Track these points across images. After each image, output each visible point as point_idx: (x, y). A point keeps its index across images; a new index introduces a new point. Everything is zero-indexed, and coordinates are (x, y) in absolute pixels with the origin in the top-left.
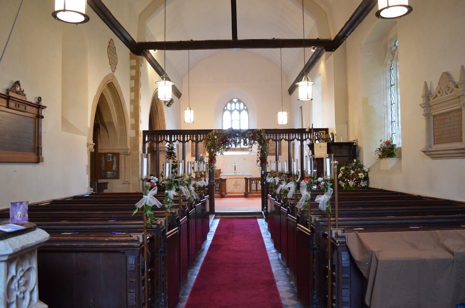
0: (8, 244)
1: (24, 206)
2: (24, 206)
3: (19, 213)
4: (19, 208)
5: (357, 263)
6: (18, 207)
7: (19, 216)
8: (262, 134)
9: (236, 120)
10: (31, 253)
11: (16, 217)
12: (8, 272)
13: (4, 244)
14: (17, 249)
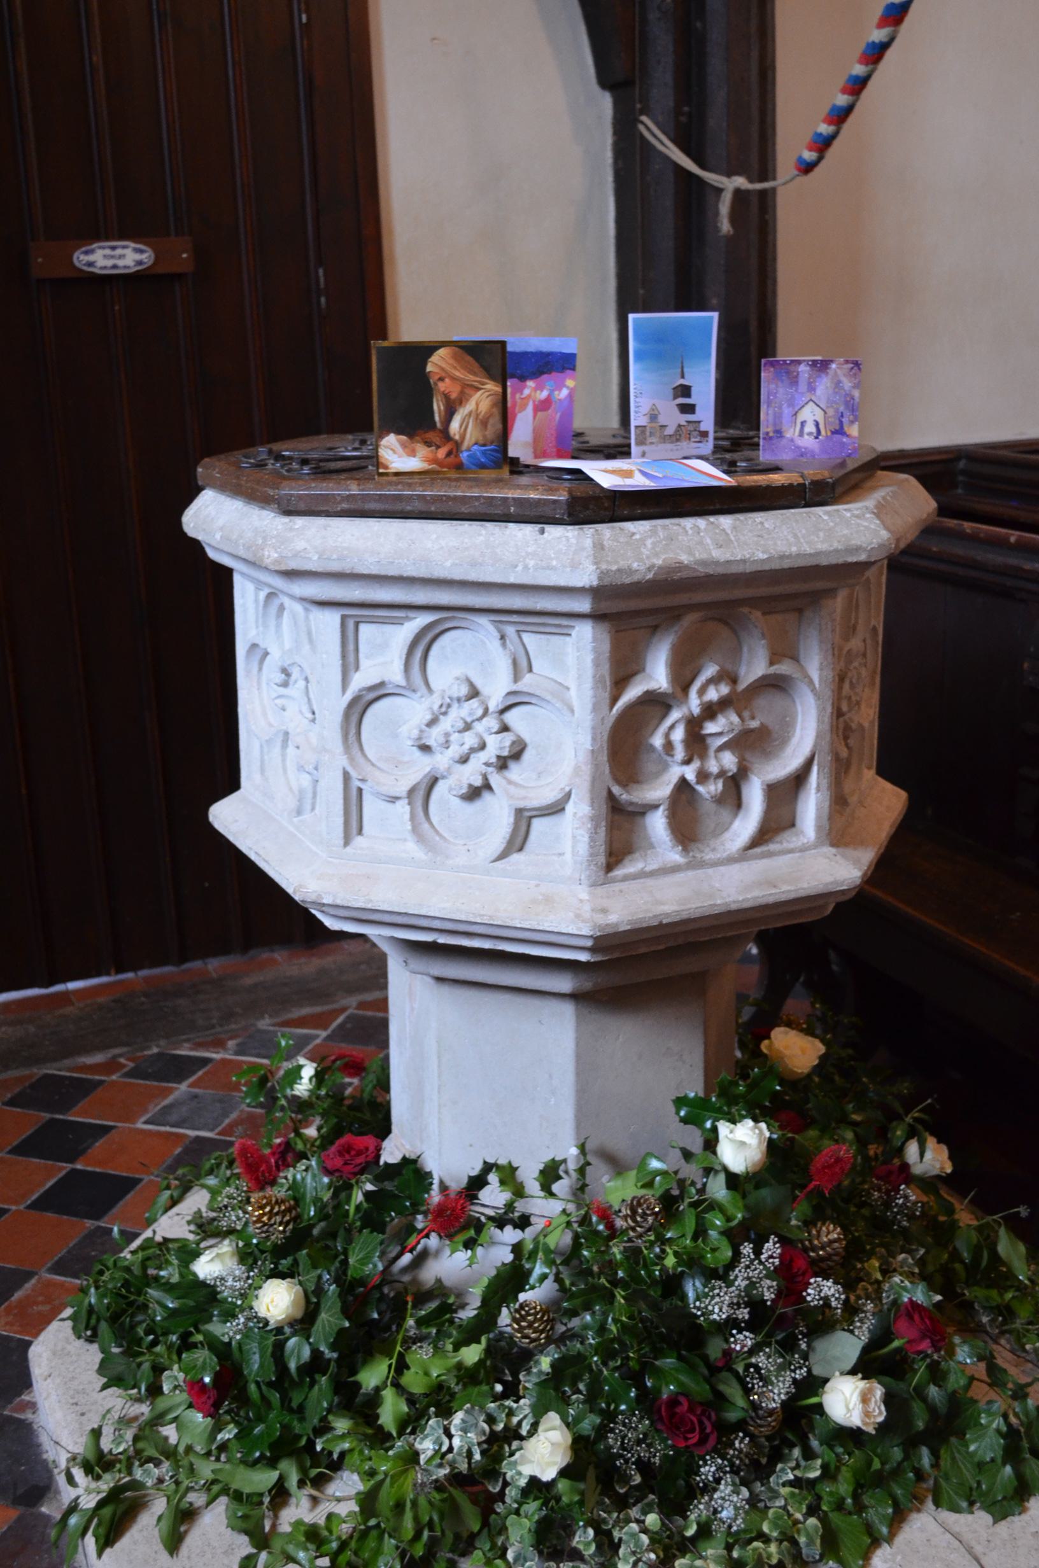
0: (588, 543)
1: (838, 384)
2: (838, 384)
3: (810, 414)
4: (812, 389)
5: (161, 270)
6: (803, 386)
7: (810, 428)
8: (410, 1218)
9: (552, 1564)
10: (800, 611)
11: (791, 433)
12: (349, 662)
13: (573, 541)
14: (631, 571)
